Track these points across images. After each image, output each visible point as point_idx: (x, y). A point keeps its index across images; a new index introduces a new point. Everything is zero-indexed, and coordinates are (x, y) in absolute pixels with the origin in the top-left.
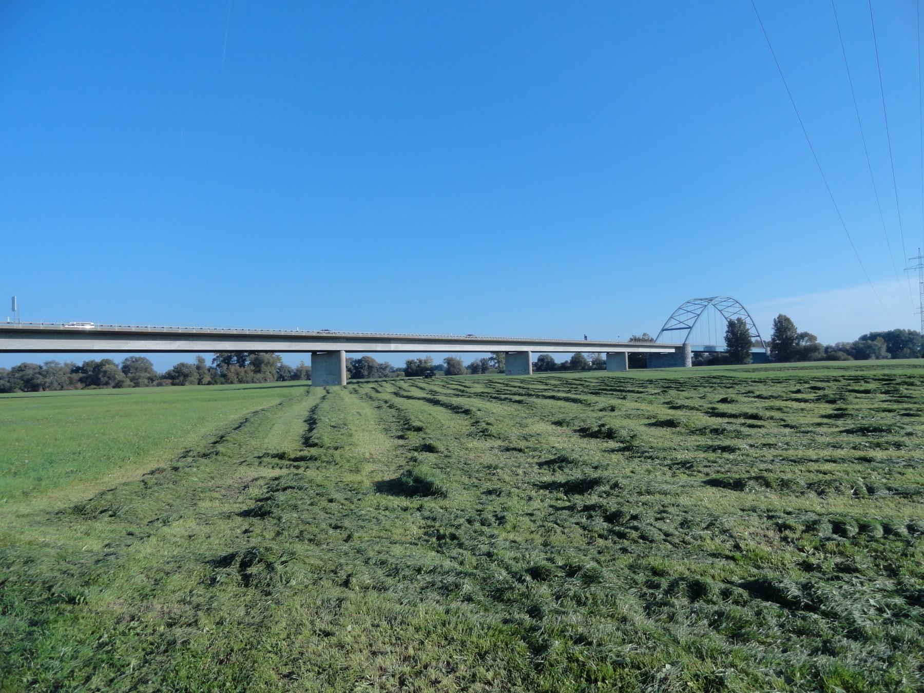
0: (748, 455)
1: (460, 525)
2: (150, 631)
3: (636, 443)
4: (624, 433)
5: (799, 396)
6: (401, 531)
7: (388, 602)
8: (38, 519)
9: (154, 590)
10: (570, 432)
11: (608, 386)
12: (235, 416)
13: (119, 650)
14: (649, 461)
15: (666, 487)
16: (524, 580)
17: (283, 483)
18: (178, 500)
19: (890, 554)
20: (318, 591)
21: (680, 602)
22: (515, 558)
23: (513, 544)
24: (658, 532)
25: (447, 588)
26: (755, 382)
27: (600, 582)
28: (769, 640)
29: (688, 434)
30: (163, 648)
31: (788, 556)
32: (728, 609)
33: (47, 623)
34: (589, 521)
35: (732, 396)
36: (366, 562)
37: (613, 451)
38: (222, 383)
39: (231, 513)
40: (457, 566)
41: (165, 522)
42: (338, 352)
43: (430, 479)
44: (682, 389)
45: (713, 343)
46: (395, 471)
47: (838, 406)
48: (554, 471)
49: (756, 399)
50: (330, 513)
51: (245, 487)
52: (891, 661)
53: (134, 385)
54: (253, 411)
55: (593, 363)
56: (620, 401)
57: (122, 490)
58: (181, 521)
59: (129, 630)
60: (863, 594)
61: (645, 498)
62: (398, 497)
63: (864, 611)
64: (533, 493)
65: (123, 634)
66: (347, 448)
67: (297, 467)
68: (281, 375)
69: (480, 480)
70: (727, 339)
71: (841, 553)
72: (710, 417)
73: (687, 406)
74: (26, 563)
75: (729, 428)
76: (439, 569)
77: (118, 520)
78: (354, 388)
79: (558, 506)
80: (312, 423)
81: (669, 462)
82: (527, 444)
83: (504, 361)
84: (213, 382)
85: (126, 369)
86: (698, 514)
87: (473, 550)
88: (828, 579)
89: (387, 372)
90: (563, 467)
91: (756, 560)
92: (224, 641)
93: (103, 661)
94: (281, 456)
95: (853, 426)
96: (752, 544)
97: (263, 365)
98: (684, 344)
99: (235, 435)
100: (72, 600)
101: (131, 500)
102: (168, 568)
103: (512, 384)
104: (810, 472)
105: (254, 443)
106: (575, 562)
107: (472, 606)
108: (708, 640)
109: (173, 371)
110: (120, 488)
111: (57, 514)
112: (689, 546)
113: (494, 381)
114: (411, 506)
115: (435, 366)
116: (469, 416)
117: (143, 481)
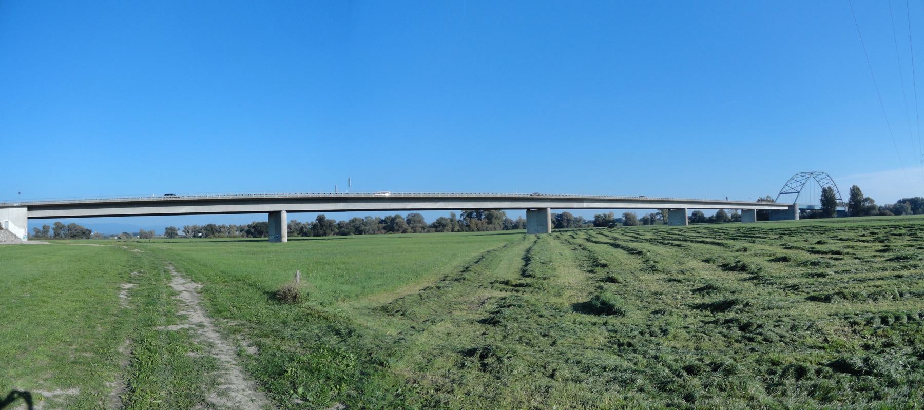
0: (833, 279)
1: (634, 336)
2: (425, 392)
3: (761, 274)
4: (753, 267)
5: (864, 238)
6: (592, 339)
7: (582, 391)
8: (363, 311)
9: (427, 366)
10: (715, 267)
11: (742, 233)
12: (475, 254)
13: (408, 400)
14: (770, 286)
15: (781, 303)
16: (682, 375)
17: (508, 302)
18: (440, 309)
19: (910, 332)
20: (532, 380)
21: (790, 381)
22: (675, 360)
23: (673, 350)
24: (776, 335)
25: (625, 382)
26: (838, 229)
27: (736, 374)
28: (844, 398)
29: (796, 266)
30: (433, 404)
31: (856, 342)
32: (820, 382)
33: (369, 374)
34: (728, 331)
35: (824, 239)
36: (567, 361)
37: (745, 280)
38: (466, 231)
39: (474, 320)
40: (632, 366)
41: (433, 322)
42: (545, 209)
43: (612, 302)
44: (792, 235)
45: (813, 204)
46: (587, 296)
47: (885, 244)
48: (703, 295)
49: (839, 241)
50: (541, 325)
51: (483, 303)
52: (909, 396)
53: (413, 232)
54: (487, 250)
55: (732, 217)
56: (750, 244)
57: (408, 299)
58: (443, 323)
59: (413, 389)
60: (896, 359)
61: (766, 312)
62: (589, 315)
63: (896, 369)
64: (688, 312)
65: (410, 390)
66: (552, 279)
67: (517, 291)
68: (506, 226)
69: (649, 303)
70: (822, 201)
71: (885, 336)
72: (810, 254)
73: (796, 247)
74: (358, 337)
75: (822, 261)
76: (619, 368)
77: (406, 318)
78: (557, 235)
79: (706, 321)
80: (527, 260)
81: (783, 286)
82: (684, 276)
83: (667, 216)
84: (461, 230)
85: (409, 221)
86: (802, 320)
87: (644, 354)
88: (878, 353)
89: (581, 223)
90: (710, 292)
91: (837, 347)
92: (470, 407)
93: (399, 405)
94: (506, 283)
95: (893, 256)
96: (835, 337)
97: (493, 219)
98: (794, 204)
99: (475, 267)
100: (381, 364)
101: (413, 305)
102: (435, 352)
103: (673, 232)
104: (869, 287)
105: (488, 273)
106: (718, 361)
107: (643, 395)
108: (807, 404)
109: (436, 222)
110: (407, 297)
111: (373, 310)
112: (796, 343)
113: (660, 230)
114: (599, 322)
115: (616, 219)
116: (641, 256)
117: (419, 294)
